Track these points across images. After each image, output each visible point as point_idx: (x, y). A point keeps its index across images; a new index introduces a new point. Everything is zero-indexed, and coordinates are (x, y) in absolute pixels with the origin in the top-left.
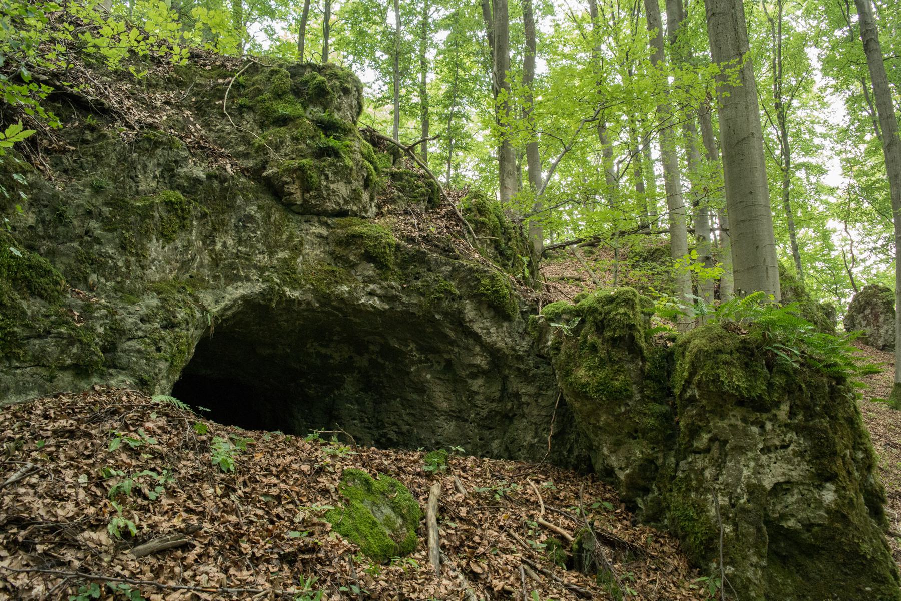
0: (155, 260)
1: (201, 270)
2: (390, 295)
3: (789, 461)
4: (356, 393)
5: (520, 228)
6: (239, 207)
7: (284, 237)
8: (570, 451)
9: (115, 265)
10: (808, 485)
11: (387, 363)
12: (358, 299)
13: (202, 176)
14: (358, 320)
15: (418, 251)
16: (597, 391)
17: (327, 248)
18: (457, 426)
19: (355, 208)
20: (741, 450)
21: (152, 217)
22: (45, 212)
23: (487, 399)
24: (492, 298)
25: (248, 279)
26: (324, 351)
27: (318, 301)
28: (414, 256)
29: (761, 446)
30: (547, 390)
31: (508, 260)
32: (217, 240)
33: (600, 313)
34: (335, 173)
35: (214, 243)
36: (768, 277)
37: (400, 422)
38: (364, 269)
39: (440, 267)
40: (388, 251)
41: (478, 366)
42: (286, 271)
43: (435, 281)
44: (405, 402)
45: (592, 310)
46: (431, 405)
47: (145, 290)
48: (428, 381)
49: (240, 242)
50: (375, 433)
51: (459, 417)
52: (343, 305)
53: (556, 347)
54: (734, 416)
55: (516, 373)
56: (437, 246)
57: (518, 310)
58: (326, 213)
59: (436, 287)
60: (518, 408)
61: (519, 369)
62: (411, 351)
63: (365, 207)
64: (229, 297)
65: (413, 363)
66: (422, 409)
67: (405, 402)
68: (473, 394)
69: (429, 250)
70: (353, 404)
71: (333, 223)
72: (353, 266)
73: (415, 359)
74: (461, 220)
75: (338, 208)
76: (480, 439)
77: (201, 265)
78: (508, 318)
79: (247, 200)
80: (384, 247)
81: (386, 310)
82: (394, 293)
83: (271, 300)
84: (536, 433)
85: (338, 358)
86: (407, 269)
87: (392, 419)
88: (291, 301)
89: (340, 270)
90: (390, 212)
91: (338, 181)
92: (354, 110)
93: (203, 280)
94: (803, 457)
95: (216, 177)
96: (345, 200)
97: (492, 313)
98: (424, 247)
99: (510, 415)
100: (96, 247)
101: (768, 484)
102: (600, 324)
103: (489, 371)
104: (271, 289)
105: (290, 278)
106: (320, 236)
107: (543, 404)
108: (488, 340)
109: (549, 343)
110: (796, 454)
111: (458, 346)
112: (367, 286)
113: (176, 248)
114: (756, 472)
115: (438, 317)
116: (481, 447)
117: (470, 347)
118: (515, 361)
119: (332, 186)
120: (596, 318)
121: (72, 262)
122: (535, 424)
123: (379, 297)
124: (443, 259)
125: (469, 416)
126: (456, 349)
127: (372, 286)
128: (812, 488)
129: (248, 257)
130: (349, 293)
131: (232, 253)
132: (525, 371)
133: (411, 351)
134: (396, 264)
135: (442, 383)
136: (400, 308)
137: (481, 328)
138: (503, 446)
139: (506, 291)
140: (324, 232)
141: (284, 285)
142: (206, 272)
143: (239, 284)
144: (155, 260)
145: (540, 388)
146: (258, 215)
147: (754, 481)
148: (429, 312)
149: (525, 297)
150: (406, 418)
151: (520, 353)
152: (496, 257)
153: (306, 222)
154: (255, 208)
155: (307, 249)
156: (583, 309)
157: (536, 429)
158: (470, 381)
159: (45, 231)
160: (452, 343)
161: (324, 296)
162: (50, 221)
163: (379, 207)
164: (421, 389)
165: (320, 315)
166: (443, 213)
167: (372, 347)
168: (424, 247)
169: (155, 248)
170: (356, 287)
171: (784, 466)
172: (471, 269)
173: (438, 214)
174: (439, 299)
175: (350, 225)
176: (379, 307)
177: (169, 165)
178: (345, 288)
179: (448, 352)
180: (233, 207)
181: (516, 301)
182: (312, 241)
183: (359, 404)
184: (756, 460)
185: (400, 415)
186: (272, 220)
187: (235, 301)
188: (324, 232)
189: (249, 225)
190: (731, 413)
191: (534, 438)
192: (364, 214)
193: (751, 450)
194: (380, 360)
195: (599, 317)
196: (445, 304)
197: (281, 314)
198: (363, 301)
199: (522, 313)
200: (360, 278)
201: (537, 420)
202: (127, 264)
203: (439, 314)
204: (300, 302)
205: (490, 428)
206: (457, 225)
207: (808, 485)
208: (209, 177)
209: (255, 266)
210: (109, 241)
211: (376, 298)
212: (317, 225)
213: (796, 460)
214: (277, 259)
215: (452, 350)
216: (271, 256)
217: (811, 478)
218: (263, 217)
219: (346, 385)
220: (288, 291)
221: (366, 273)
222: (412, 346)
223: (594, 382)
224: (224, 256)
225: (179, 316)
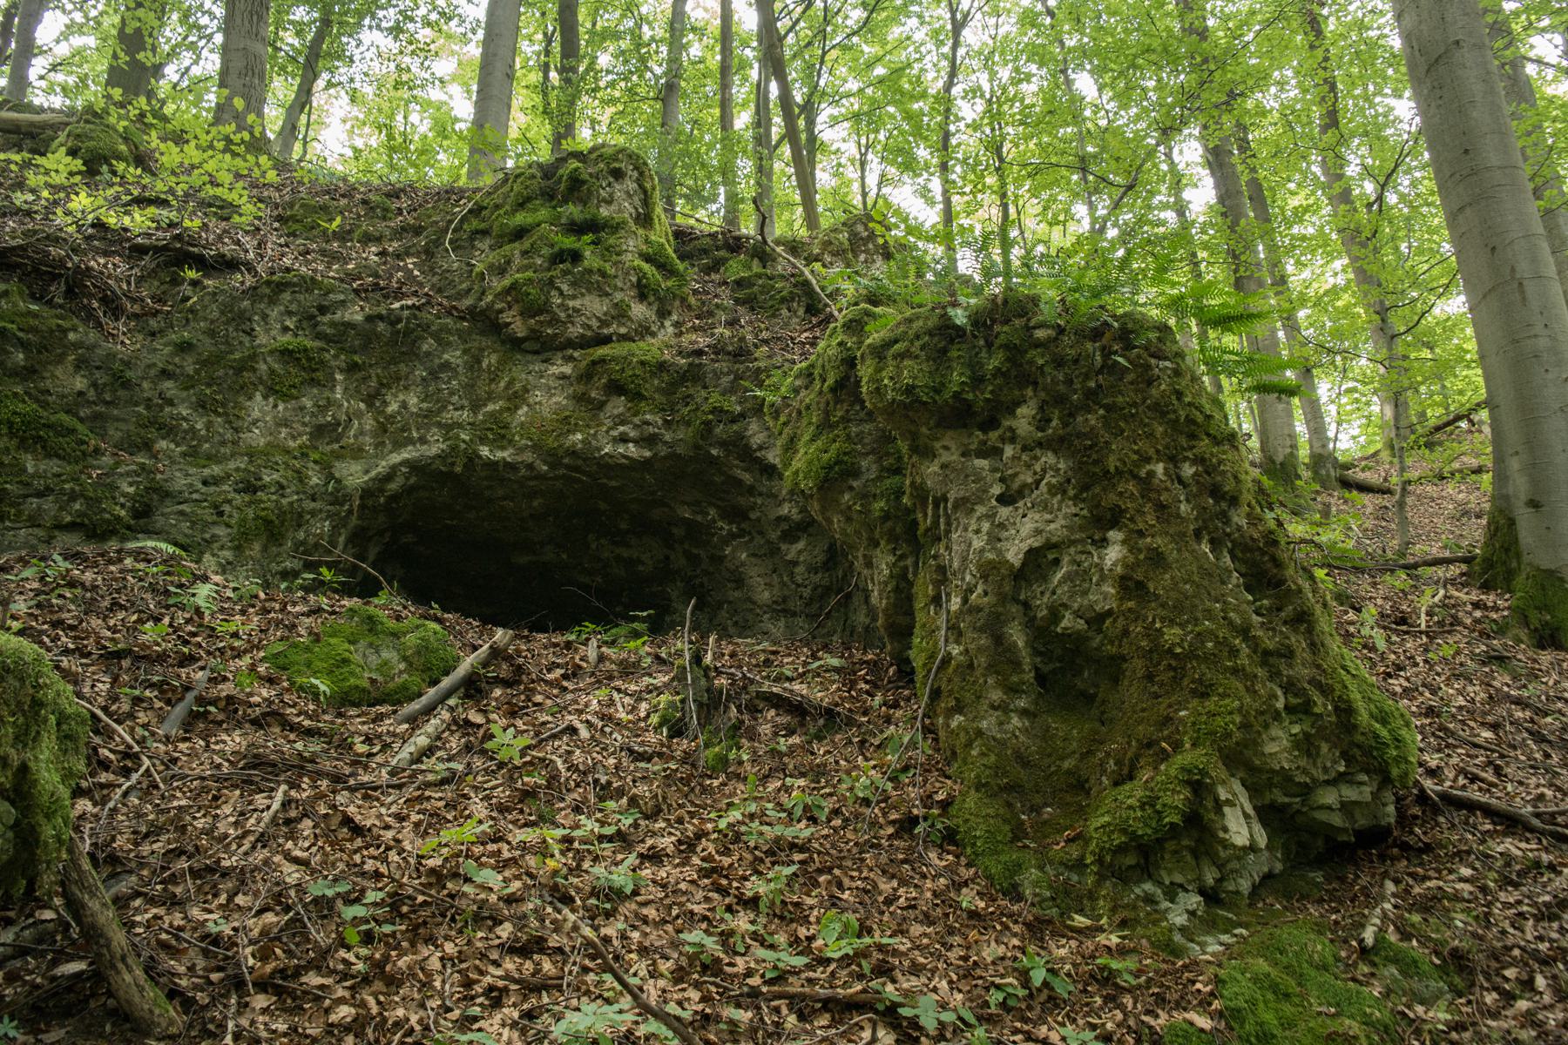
2: (646, 434)
3: (1046, 507)
6: (428, 354)
7: (502, 384)
9: (193, 428)
10: (1082, 541)
12: (599, 449)
14: (614, 483)
19: (623, 330)
20: (965, 505)
21: (254, 370)
22: (98, 374)
25: (423, 441)
27: (545, 462)
29: (997, 490)
32: (388, 398)
34: (573, 284)
35: (385, 403)
36: (1524, 299)
48: (743, 564)
52: (580, 462)
54: (946, 448)
58: (570, 344)
62: (714, 521)
72: (601, 405)
75: (589, 333)
77: (361, 432)
79: (444, 345)
82: (651, 429)
83: (453, 464)
88: (492, 465)
91: (583, 295)
92: (636, 199)
94: (1064, 492)
100: (168, 409)
101: (1014, 554)
104: (454, 448)
106: (563, 377)
110: (1053, 490)
111: (760, 494)
113: (302, 408)
114: (994, 539)
115: (714, 452)
119: (571, 304)
121: (132, 428)
123: (635, 442)
128: (1089, 547)
130: (582, 441)
133: (714, 521)
135: (759, 561)
136: (663, 451)
140: (567, 369)
147: (990, 556)
155: (538, 395)
158: (784, 547)
159: (99, 394)
160: (751, 490)
162: (105, 385)
169: (258, 406)
171: (1037, 516)
176: (635, 456)
178: (579, 436)
180: (417, 355)
184: (991, 516)
188: (567, 369)
190: (937, 445)
193: (981, 501)
196: (719, 430)
197: (489, 487)
202: (209, 425)
207: (1082, 541)
208: (369, 319)
209: (439, 425)
210: (183, 401)
213: (1055, 501)
216: (475, 408)
217: (1081, 528)
218: (466, 363)
220: (485, 451)
222: (712, 512)
225: (267, 479)
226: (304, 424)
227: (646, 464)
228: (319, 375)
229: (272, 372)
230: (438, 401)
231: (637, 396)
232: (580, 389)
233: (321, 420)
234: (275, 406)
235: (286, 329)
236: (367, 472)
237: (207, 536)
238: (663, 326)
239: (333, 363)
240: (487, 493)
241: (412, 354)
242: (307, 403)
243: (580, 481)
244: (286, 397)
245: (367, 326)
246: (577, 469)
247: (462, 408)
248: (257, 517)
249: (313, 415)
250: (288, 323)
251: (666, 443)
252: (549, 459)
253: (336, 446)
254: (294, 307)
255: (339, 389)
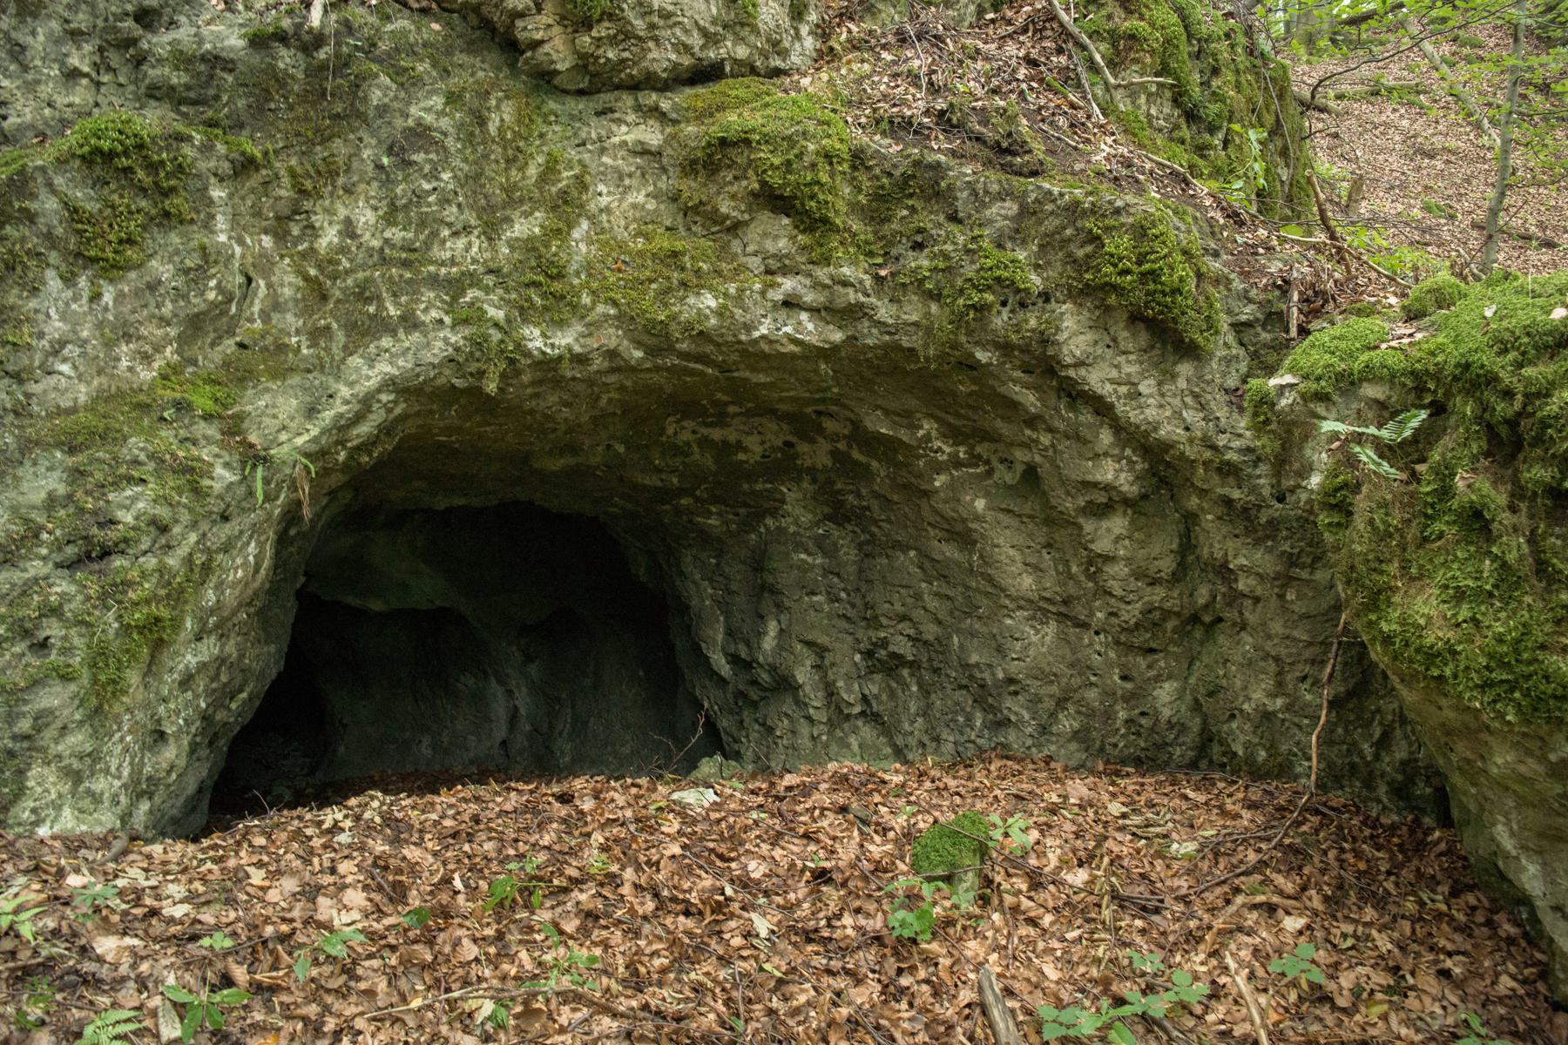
0: (63, 343)
1: (275, 317)
2: (840, 303)
4: (817, 524)
5: (1249, 31)
6: (383, 110)
7: (532, 171)
8: (1384, 743)
11: (875, 464)
12: (748, 328)
13: (234, 42)
15: (917, 164)
16: (1486, 685)
17: (662, 185)
18: (1062, 638)
19: (742, 52)
21: (31, 217)
23: (1139, 575)
24: (1139, 296)
25: (409, 322)
26: (716, 434)
27: (639, 344)
28: (906, 178)
30: (1313, 569)
31: (1212, 130)
32: (317, 219)
33: (1508, 394)
35: (311, 230)
37: (918, 614)
38: (765, 235)
39: (984, 205)
40: (824, 178)
41: (1108, 488)
42: (530, 276)
43: (968, 251)
44: (927, 564)
45: (1472, 380)
46: (990, 580)
47: (27, 446)
48: (978, 518)
49: (391, 215)
50: (860, 634)
51: (1066, 616)
52: (709, 349)
53: (1339, 501)
55: (1219, 511)
56: (978, 138)
57: (1224, 322)
58: (649, 82)
59: (969, 270)
60: (1229, 604)
61: (1228, 502)
62: (928, 438)
63: (776, 44)
64: (345, 391)
65: (938, 468)
66: (968, 588)
67: (927, 564)
68: (1096, 563)
69: (953, 153)
70: (809, 554)
71: (676, 108)
72: (735, 228)
73: (942, 458)
74: (1070, 35)
76: (1124, 678)
77: (276, 305)
78: (1191, 351)
79: (408, 82)
80: (813, 166)
81: (836, 348)
82: (852, 296)
83: (481, 374)
84: (1280, 685)
85: (758, 449)
86: (888, 220)
87: (898, 607)
88: (547, 366)
89: (695, 245)
90: (854, 45)
93: (281, 348)
95: (282, 37)
96: (704, 33)
97: (1144, 338)
98: (939, 148)
99: (1207, 619)
102: (1504, 431)
103: (1144, 497)
104: (478, 343)
105: (544, 296)
106: (643, 151)
107: (1299, 608)
108: (1134, 416)
109: (1315, 480)
111: (1050, 430)
112: (773, 285)
113: (153, 287)
115: (982, 356)
116: (1125, 699)
117: (1084, 432)
118: (1216, 479)
120: (1486, 407)
122: (1277, 659)
123: (814, 310)
124: (993, 180)
125: (1091, 615)
126: (1045, 439)
127: (788, 284)
129: (412, 257)
130: (720, 313)
131: (370, 251)
132: (1245, 510)
134: (854, 207)
135: (1014, 522)
136: (872, 337)
137: (1112, 381)
138: (1188, 698)
139: (1183, 270)
140: (652, 135)
141: (525, 321)
142: (292, 321)
143: (386, 342)
144: (63, 343)
145: (1292, 561)
146: (445, 123)
148: (955, 346)
149: (1245, 275)
150: (932, 604)
151: (1231, 456)
152: (1177, 127)
153: (599, 114)
154: (438, 101)
155: (603, 195)
156: (1440, 368)
157: (1279, 674)
158: (1088, 526)
160: (1032, 421)
161: (651, 327)
163: (823, 32)
164: (963, 536)
165: (656, 378)
166: (1020, 21)
167: (829, 425)
168: (939, 148)
170: (741, 291)
172: (1077, 203)
173: (1009, 22)
174: (981, 309)
175: (721, 108)
176: (813, 340)
177: (116, 30)
178: (709, 301)
179: (1027, 445)
181: (1216, 293)
182: (617, 170)
183: (825, 554)
185: (918, 596)
186: (492, 128)
187: (367, 402)
188: (652, 135)
189: (419, 157)
191: (1274, 696)
192: (777, 62)
194: (856, 455)
195: (1501, 408)
196: (1000, 320)
197: (536, 395)
198: (763, 330)
199: (1239, 327)
200: (755, 263)
201: (1283, 652)
203: (984, 347)
204: (580, 360)
205: (1152, 651)
206: (1060, 51)
208: (259, 41)
209: (434, 281)
211: (804, 316)
212: (631, 118)
214: (510, 244)
215: (1037, 441)
216: (491, 231)
218: (460, 127)
219: (788, 507)
221: (771, 246)
222: (928, 426)
223: (1474, 653)
224: (346, 264)
225: (128, 518)
226: (164, 321)
227: (829, 353)
228: (176, 203)
229: (73, 212)
230: (422, 224)
231: (813, 223)
232: (692, 189)
233: (197, 303)
234: (96, 297)
235: (72, 75)
236: (311, 412)
237: (25, 725)
238: (798, 37)
239: (203, 165)
240: (528, 405)
241: (354, 115)
242: (162, 269)
243: (702, 373)
244: (112, 269)
245: (256, 60)
246: (699, 358)
247: (467, 229)
248: (126, 629)
249: (179, 295)
250: (74, 61)
251: (880, 324)
252: (646, 339)
253: (229, 345)
254: (81, 20)
255: (221, 222)
